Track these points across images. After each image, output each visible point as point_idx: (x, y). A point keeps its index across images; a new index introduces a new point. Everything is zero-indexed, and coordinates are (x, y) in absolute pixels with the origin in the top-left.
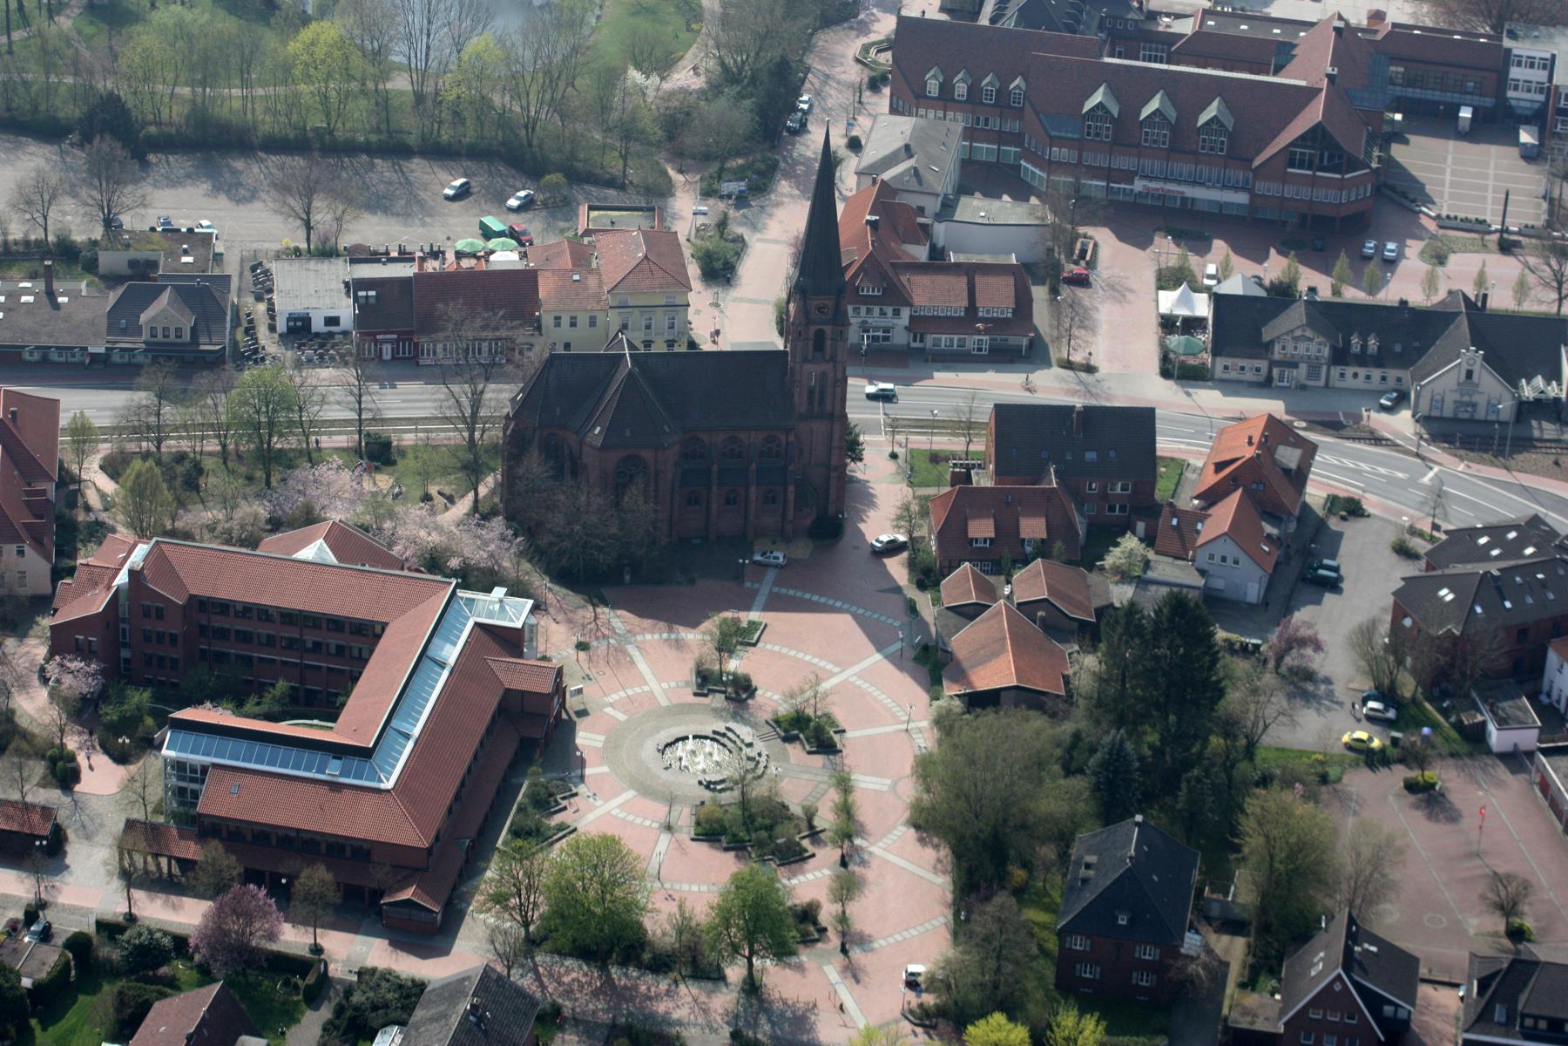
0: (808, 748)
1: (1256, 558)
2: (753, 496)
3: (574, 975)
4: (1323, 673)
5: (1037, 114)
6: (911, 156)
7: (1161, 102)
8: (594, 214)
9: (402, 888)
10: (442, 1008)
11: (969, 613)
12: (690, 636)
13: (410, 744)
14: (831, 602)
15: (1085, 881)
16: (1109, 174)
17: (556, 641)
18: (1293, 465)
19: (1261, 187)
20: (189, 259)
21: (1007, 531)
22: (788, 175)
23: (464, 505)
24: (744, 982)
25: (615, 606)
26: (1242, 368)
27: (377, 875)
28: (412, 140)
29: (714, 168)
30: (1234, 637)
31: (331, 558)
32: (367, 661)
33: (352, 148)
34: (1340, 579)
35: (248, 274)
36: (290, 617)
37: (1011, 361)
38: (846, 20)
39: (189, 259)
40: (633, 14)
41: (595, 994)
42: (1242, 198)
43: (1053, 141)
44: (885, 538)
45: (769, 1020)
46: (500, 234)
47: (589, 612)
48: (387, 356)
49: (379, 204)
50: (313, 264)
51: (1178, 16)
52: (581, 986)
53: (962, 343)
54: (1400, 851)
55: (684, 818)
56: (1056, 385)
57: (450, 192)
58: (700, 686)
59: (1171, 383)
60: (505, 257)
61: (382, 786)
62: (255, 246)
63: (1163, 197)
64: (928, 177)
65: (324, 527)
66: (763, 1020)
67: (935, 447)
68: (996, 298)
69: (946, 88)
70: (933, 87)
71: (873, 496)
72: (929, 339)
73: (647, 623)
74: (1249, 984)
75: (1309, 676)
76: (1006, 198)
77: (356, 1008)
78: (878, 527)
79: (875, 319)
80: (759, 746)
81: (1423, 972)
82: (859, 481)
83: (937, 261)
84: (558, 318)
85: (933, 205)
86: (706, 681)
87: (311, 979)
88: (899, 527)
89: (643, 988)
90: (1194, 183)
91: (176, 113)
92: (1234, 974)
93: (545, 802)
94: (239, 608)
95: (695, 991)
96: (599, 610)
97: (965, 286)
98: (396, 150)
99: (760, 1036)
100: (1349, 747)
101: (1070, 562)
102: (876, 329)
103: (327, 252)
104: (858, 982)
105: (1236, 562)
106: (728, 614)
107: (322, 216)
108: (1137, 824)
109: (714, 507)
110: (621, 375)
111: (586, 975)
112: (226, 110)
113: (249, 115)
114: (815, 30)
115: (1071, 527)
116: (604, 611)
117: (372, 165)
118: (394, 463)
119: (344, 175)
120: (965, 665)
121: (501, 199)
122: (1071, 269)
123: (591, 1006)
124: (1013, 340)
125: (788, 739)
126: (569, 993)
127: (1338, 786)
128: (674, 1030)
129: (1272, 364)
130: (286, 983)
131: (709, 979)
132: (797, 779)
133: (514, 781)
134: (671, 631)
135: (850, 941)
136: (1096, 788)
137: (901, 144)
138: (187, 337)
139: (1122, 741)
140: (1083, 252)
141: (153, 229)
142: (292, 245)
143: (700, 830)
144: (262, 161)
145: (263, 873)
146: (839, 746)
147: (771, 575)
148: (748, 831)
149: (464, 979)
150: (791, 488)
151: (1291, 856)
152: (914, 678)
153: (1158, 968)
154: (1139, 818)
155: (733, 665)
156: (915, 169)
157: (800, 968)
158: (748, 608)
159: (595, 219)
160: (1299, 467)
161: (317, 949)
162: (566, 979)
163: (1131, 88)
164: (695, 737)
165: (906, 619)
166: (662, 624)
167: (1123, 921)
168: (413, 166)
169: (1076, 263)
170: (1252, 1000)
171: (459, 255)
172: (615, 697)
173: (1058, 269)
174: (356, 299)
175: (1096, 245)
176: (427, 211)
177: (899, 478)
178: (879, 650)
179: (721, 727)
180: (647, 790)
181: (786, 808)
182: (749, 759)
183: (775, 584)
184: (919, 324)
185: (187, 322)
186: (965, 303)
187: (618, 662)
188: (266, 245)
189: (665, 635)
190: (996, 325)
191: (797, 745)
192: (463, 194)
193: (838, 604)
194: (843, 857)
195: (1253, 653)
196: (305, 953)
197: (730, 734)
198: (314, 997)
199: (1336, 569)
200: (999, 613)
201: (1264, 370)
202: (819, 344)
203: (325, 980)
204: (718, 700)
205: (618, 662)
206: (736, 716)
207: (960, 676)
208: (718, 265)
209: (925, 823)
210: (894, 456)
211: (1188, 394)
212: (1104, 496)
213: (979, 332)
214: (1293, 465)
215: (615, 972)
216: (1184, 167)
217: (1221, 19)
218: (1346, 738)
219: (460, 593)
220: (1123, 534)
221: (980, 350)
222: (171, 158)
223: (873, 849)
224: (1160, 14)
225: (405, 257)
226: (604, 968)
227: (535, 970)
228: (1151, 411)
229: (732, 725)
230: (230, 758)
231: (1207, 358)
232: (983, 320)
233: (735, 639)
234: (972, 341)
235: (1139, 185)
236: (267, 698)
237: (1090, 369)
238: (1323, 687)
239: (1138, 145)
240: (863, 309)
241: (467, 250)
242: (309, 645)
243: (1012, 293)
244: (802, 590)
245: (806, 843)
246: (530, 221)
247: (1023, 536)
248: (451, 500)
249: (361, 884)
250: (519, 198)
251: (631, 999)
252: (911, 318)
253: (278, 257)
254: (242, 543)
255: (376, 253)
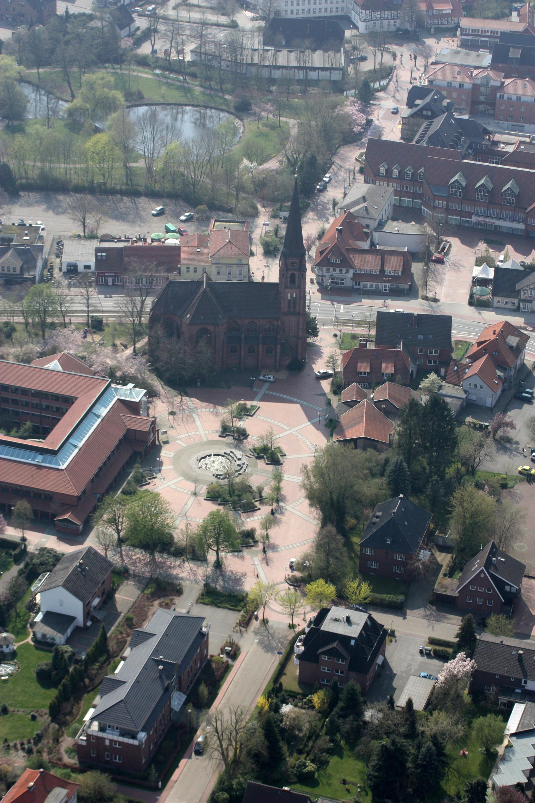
0: (267, 462)
1: (492, 387)
2: (260, 349)
3: (138, 556)
4: (516, 439)
5: (428, 184)
6: (365, 201)
7: (459, 176)
8: (217, 223)
9: (65, 513)
10: (67, 565)
11: (350, 404)
12: (220, 409)
13: (77, 450)
14: (292, 398)
15: (374, 523)
16: (461, 213)
17: (160, 409)
18: (514, 345)
19: (530, 221)
20: (27, 238)
21: (375, 370)
22: (313, 210)
23: (129, 351)
24: (215, 562)
25: (190, 396)
26: (506, 302)
27: (53, 508)
28: (142, 189)
29: (278, 205)
30: (476, 421)
31: (60, 369)
32: (65, 413)
33: (113, 192)
34: (532, 397)
35: (55, 246)
36: (39, 394)
37: (400, 296)
38: (356, 141)
39: (27, 238)
40: (257, 137)
41: (146, 564)
42: (522, 226)
43: (436, 197)
44: (322, 371)
45: (223, 580)
46: (174, 231)
47: (178, 399)
48: (110, 283)
49: (121, 217)
50: (83, 242)
51: (508, 144)
52: (140, 561)
53: (377, 287)
54: (523, 517)
55: (203, 490)
56: (419, 307)
57: (155, 212)
58: (223, 432)
59: (472, 308)
60: (172, 241)
61: (60, 468)
62: (60, 234)
63: (486, 225)
64: (371, 210)
65: (59, 355)
66: (220, 579)
67: (354, 332)
68: (394, 266)
69: (389, 172)
70: (382, 170)
71: (322, 353)
72: (362, 284)
73: (204, 404)
74: (450, 574)
75: (509, 440)
76: (413, 223)
77: (34, 565)
78: (320, 367)
79: (337, 274)
80: (244, 460)
81: (526, 572)
82: (316, 346)
83: (372, 250)
84: (188, 268)
85: (374, 224)
86: (225, 430)
87: (17, 551)
88: (329, 366)
89: (168, 563)
90: (500, 219)
91: (34, 174)
92: (443, 571)
93: (140, 481)
94: (13, 389)
95: (192, 565)
96: (184, 398)
97: (380, 260)
98: (133, 193)
99: (217, 586)
100: (520, 472)
101: (404, 385)
102: (337, 278)
103: (92, 237)
104: (268, 565)
105: (481, 388)
106: (242, 402)
107: (90, 221)
108: (401, 498)
109: (243, 353)
110: (201, 291)
111: (143, 556)
112: (58, 173)
113: (68, 176)
114: (340, 146)
115: (406, 368)
116: (186, 399)
117: (122, 200)
118: (103, 330)
119: (108, 204)
120: (344, 427)
121: (177, 216)
122: (436, 255)
123: (143, 570)
124: (401, 286)
125: (259, 458)
126: (134, 563)
127: (512, 490)
128: (178, 582)
129: (520, 300)
130: (7, 553)
131: (199, 560)
132: (259, 476)
133: (128, 471)
134: (215, 408)
135: (268, 547)
136: (389, 484)
137: (361, 196)
138: (18, 271)
139: (401, 462)
140: (444, 248)
141: (13, 224)
142: (77, 234)
143: (209, 495)
144: (72, 196)
145: (5, 505)
146: (281, 462)
147: (266, 385)
148: (231, 497)
149: (79, 553)
150: (279, 346)
151: (472, 516)
152: (323, 433)
153: (403, 564)
154: (402, 496)
155: (240, 424)
156: (366, 207)
157: (242, 558)
158: (252, 399)
159: (217, 226)
160: (518, 346)
161: (24, 539)
162: (134, 558)
163: (472, 174)
164: (215, 455)
165: (325, 408)
166: (211, 405)
167: (388, 542)
168: (141, 201)
169: (440, 253)
170: (447, 581)
171: (153, 240)
172: (183, 436)
173: (431, 256)
174: (96, 256)
175: (450, 245)
176: (143, 220)
177: (335, 345)
178: (309, 421)
179: (228, 451)
180: (188, 477)
181: (251, 487)
182: (239, 465)
183: (267, 390)
184: (358, 277)
185: (18, 264)
186: (379, 268)
187: (187, 420)
188: (66, 233)
189: (211, 410)
190: (394, 279)
191: (262, 461)
192: (161, 213)
193: (295, 400)
194: (272, 510)
195: (484, 429)
196: (18, 540)
197: (232, 454)
198: (17, 560)
199: (531, 394)
200: (364, 405)
201: (516, 304)
202: (293, 281)
203: (24, 552)
204: (229, 439)
205: (187, 420)
206: (237, 447)
207: (341, 432)
208: (271, 248)
209: (315, 498)
210: (335, 336)
211: (480, 313)
212: (426, 356)
213: (385, 282)
214: (514, 345)
215: (157, 555)
216: (496, 211)
217: (528, 146)
218: (519, 469)
219: (113, 385)
220: (430, 373)
221: (385, 290)
222: (31, 194)
223: (287, 507)
224: (500, 142)
225: (127, 240)
226: (152, 554)
227: (121, 553)
228: (451, 317)
229: (233, 450)
230: (5, 455)
231: (490, 296)
232: (387, 276)
233: (244, 412)
234: (381, 286)
235: (474, 219)
236: (22, 430)
237: (436, 300)
238: (514, 446)
239: (501, 204)
240: (331, 269)
241: (156, 238)
242: (44, 407)
243: (401, 264)
244: (279, 393)
245: (257, 504)
246: (190, 226)
247: (382, 372)
248: (126, 347)
249: (44, 511)
250: (186, 216)
251: (162, 568)
252: (354, 274)
253: (70, 238)
254: (23, 361)
255: (115, 238)
